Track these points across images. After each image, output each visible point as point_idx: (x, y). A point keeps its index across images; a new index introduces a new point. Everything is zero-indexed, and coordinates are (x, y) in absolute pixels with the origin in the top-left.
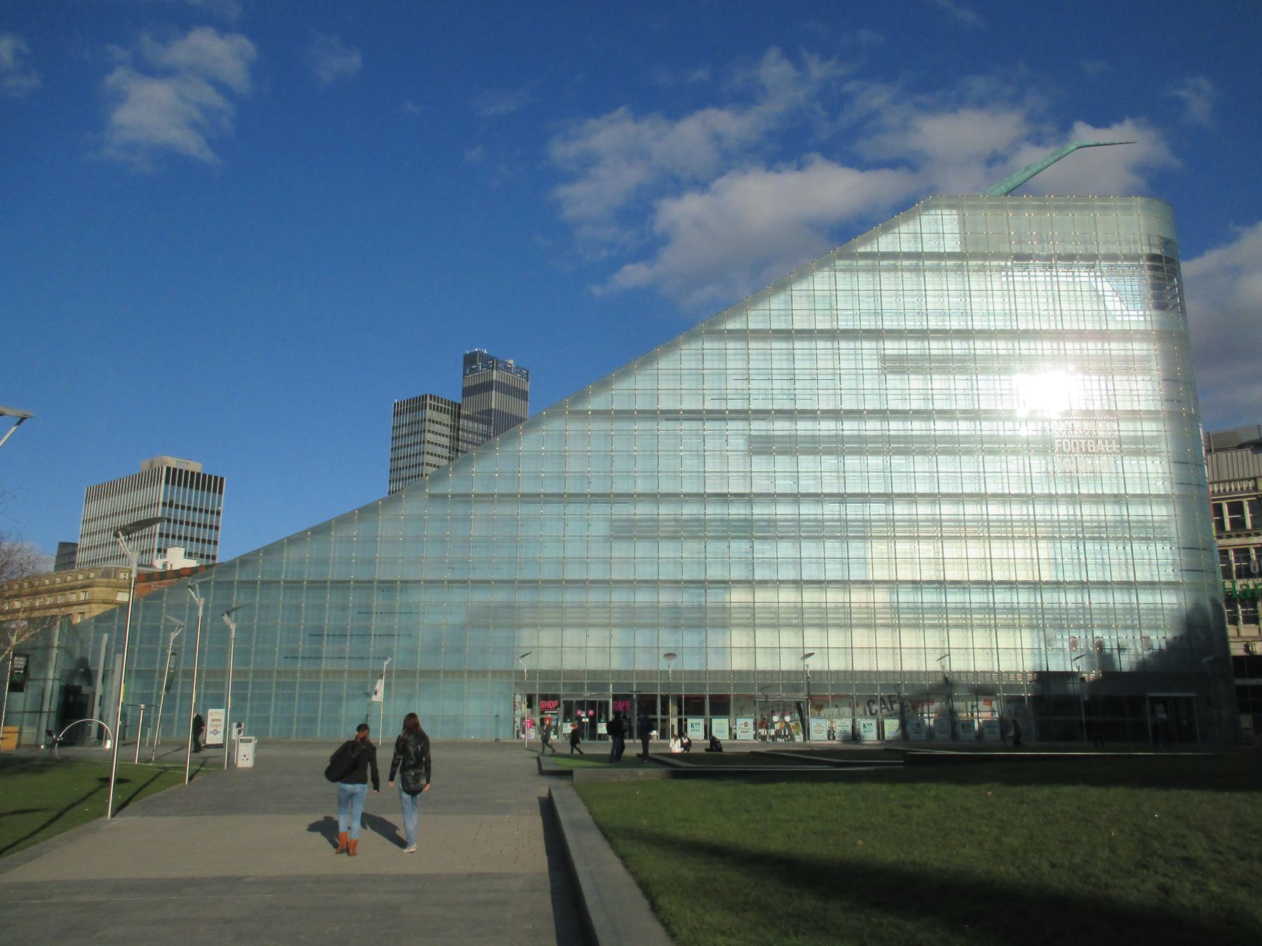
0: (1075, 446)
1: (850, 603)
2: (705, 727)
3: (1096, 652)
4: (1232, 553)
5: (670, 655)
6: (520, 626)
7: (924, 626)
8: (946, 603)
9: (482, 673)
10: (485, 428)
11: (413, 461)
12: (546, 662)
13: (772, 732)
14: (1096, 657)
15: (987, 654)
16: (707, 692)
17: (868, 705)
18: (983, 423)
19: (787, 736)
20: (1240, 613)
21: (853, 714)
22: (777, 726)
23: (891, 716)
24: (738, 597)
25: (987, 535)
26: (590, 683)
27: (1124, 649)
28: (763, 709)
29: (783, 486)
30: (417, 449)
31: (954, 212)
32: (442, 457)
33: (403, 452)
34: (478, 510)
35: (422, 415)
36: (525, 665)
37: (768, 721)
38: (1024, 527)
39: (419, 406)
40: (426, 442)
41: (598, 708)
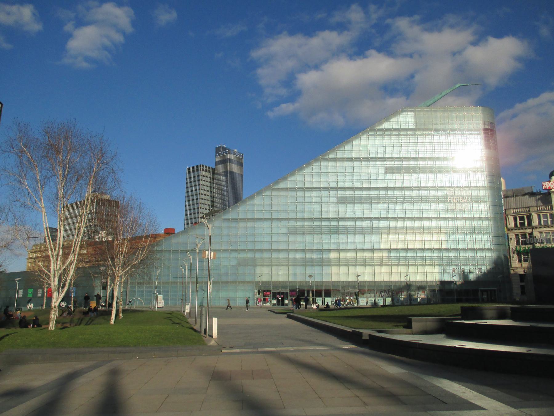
0: (455, 200)
1: (374, 257)
2: (323, 301)
3: (462, 274)
4: (520, 235)
5: (310, 276)
6: (256, 266)
7: (400, 265)
8: (408, 257)
9: (243, 283)
10: (225, 178)
11: (195, 192)
12: (266, 278)
13: (346, 303)
14: (462, 275)
15: (431, 275)
16: (323, 289)
17: (381, 293)
18: (422, 191)
19: (352, 304)
20: (523, 258)
21: (375, 296)
22: (348, 301)
23: (388, 297)
24: (334, 255)
25: (423, 232)
26: (282, 286)
27: (472, 273)
28: (343, 295)
29: (350, 215)
30: (197, 188)
31: (412, 113)
32: (207, 191)
33: (191, 189)
34: (241, 224)
35: (199, 173)
36: (257, 279)
37: (345, 299)
38: (437, 229)
39: (197, 169)
40: (201, 185)
41: (285, 295)
